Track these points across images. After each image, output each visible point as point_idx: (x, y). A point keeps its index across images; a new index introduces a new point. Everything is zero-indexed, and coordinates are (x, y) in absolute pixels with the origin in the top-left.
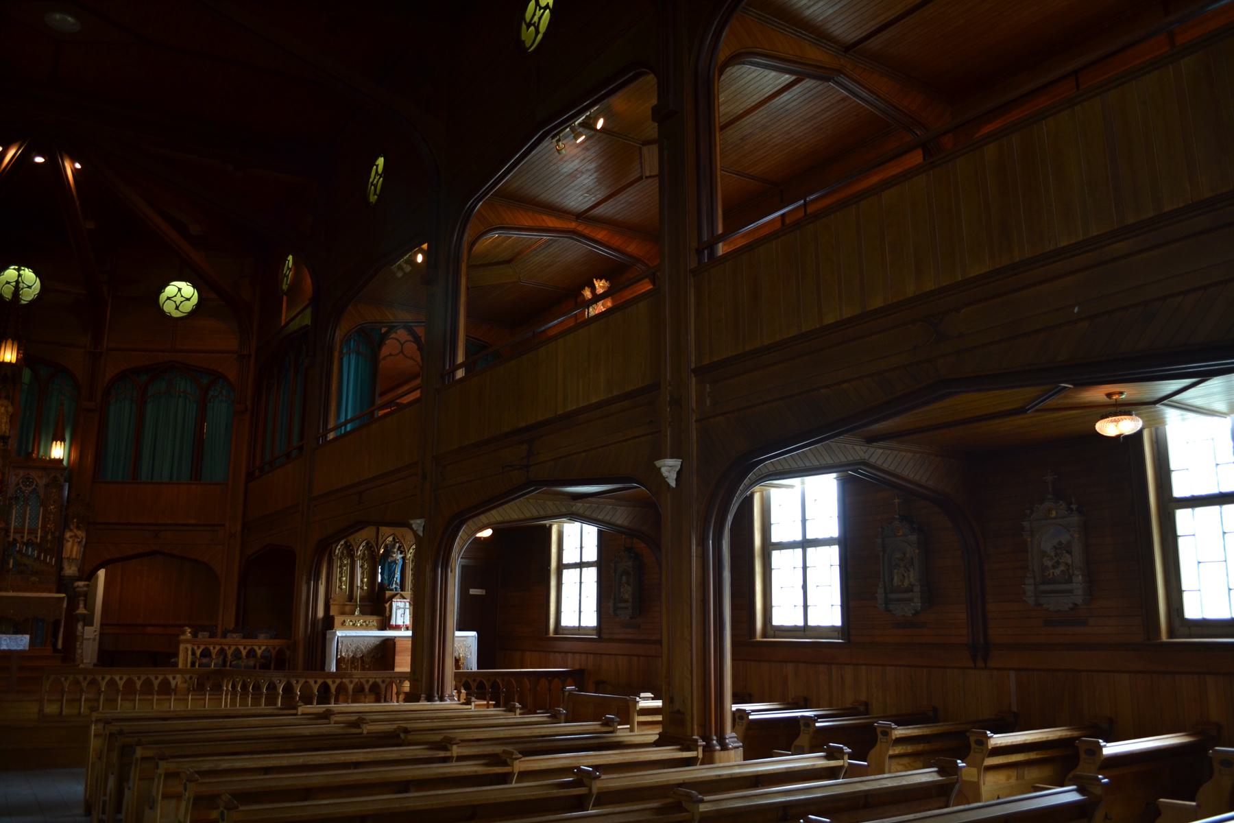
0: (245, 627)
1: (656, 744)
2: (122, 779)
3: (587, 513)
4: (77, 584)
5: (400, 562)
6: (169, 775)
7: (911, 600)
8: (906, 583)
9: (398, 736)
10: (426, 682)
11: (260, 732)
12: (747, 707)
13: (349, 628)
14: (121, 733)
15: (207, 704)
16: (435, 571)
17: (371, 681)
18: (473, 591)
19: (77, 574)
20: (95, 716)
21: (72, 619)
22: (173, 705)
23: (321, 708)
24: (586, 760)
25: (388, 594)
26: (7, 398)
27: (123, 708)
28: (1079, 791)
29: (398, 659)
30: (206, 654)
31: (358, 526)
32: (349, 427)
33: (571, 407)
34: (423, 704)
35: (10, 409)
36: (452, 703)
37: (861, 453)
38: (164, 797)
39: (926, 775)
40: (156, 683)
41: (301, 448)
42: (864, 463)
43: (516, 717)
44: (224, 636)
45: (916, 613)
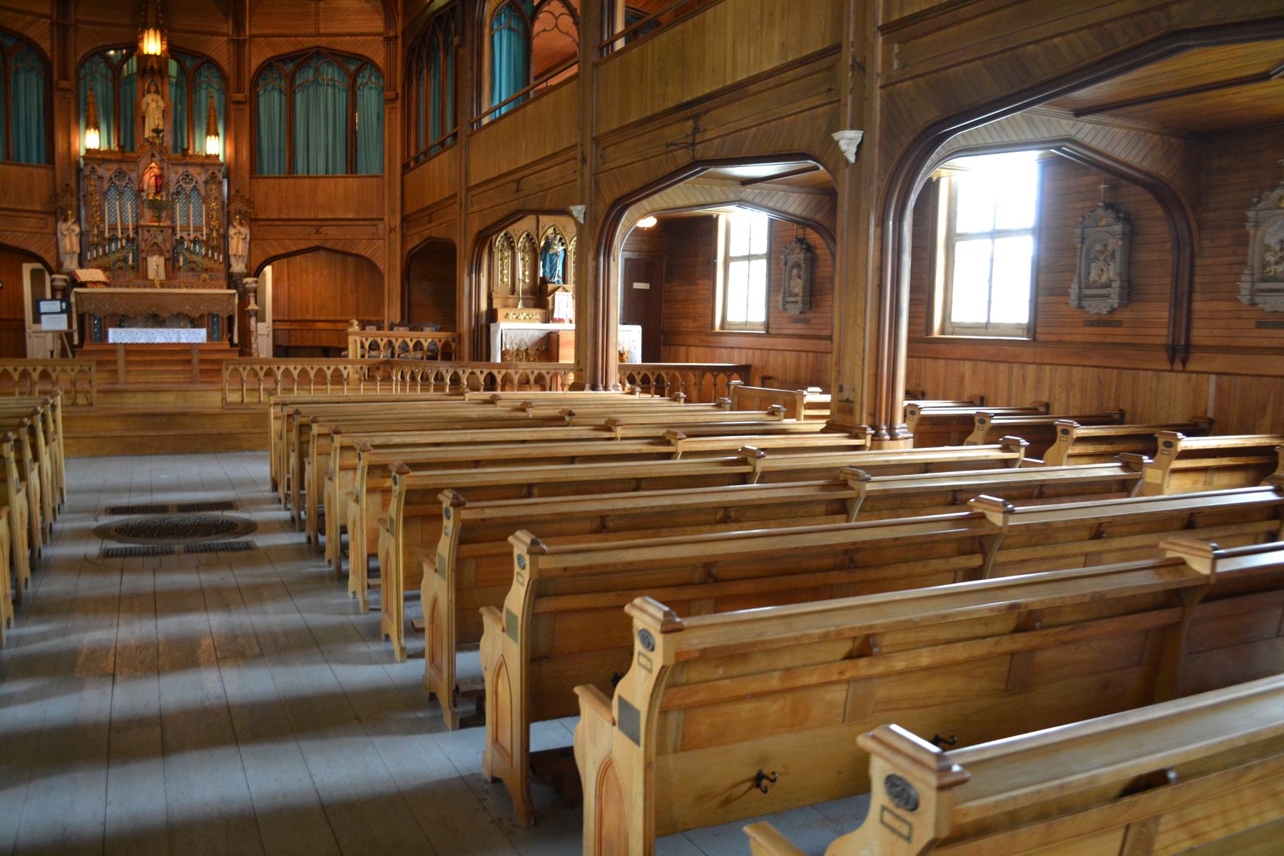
0: (410, 319)
1: (822, 431)
2: (302, 456)
3: (757, 200)
4: (245, 280)
5: (562, 255)
6: (343, 448)
7: (1107, 296)
8: (1104, 278)
9: (563, 419)
10: (590, 373)
11: (428, 413)
12: (921, 403)
13: (512, 320)
14: (297, 412)
15: (378, 390)
16: (596, 259)
17: (536, 372)
18: (637, 285)
19: (245, 271)
20: (272, 400)
21: (245, 315)
22: (346, 392)
23: (487, 395)
24: (752, 443)
25: (550, 287)
26: (157, 92)
27: (297, 394)
28: (1276, 491)
29: (562, 352)
30: (374, 346)
31: (516, 215)
32: (504, 110)
33: (742, 76)
34: (587, 393)
35: (161, 104)
36: (616, 393)
37: (1067, 128)
38: (342, 469)
39: (1109, 470)
40: (329, 373)
41: (455, 136)
42: (1070, 140)
43: (681, 406)
44: (391, 328)
45: (1113, 311)
